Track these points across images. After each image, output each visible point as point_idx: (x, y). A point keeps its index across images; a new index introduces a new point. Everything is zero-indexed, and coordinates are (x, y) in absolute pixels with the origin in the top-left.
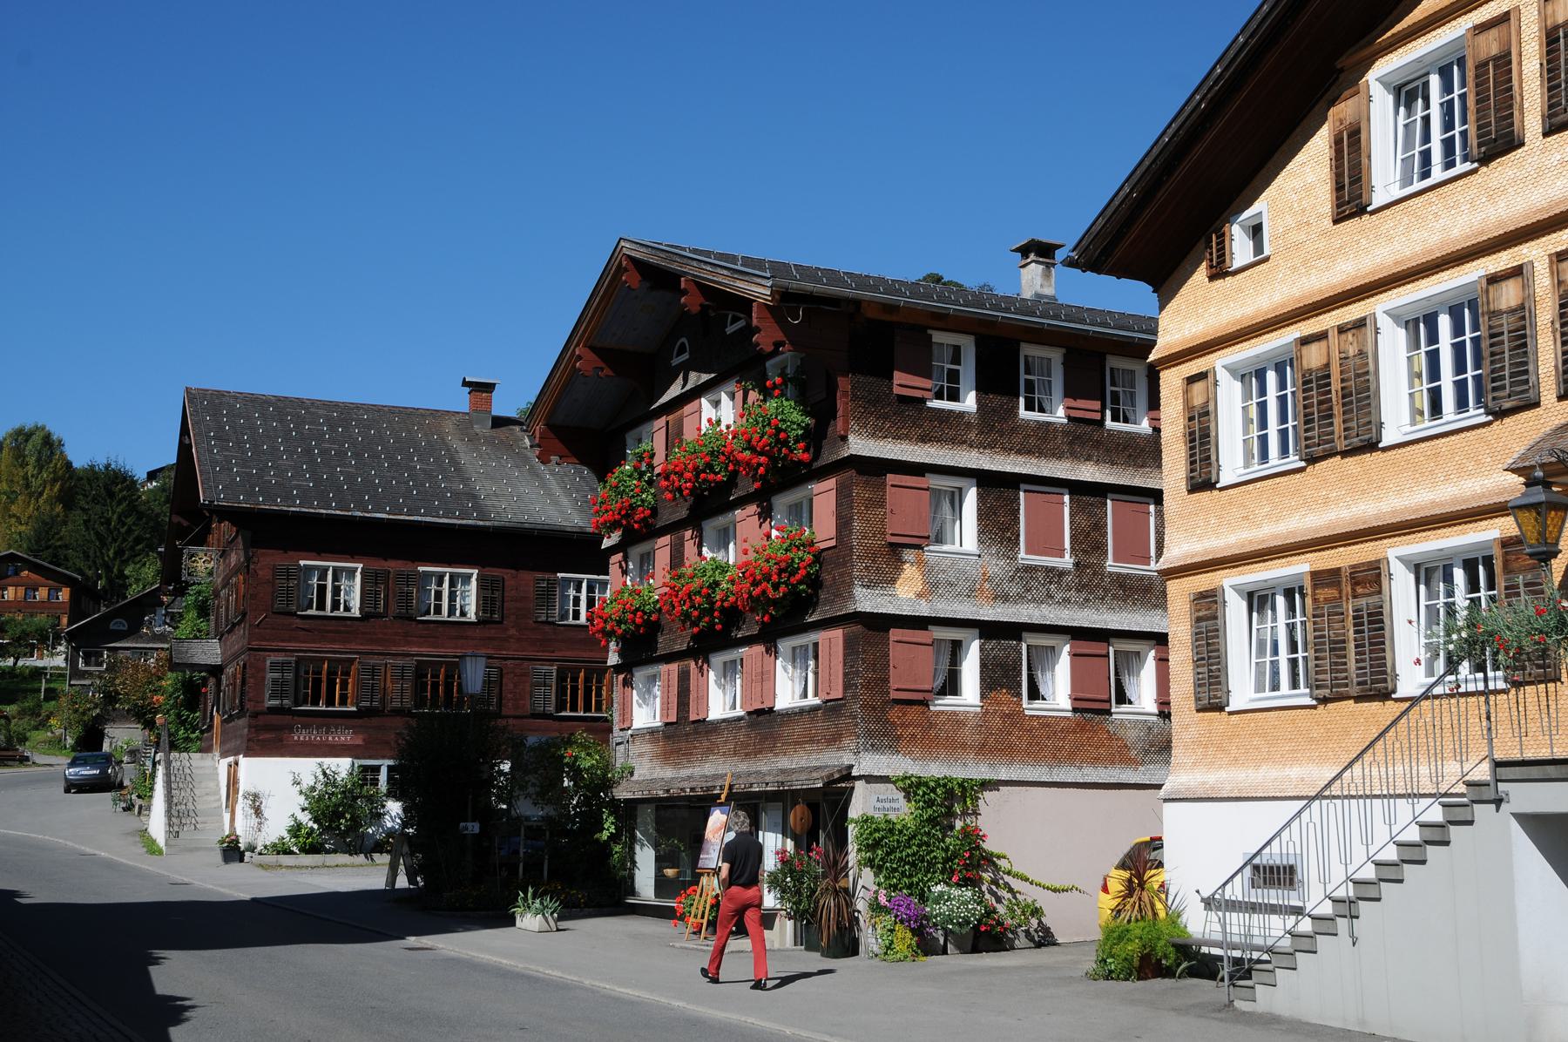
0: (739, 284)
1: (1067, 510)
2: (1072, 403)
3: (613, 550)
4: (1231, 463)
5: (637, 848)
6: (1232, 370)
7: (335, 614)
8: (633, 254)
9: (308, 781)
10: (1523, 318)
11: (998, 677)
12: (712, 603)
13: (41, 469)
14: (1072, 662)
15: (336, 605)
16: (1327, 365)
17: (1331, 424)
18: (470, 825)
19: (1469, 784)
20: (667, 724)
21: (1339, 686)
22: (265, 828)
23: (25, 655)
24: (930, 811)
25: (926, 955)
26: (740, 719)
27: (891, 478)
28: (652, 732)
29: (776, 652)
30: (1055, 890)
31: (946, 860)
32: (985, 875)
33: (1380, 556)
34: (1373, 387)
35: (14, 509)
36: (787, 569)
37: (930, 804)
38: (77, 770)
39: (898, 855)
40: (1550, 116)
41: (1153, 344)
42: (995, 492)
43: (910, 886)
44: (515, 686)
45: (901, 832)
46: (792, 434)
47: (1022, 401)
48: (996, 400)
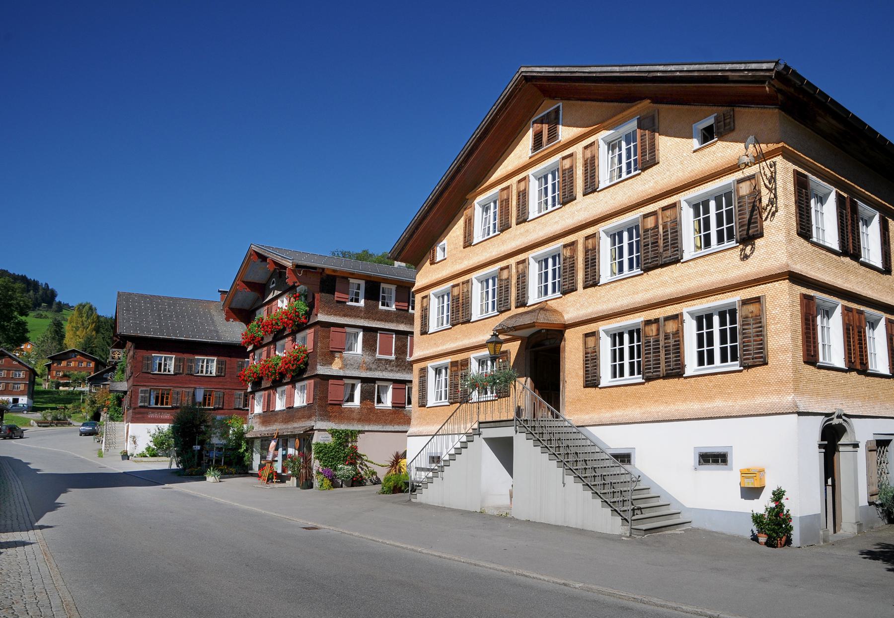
0: (283, 261)
1: (394, 340)
2: (398, 304)
3: (251, 352)
4: (433, 327)
5: (254, 454)
6: (435, 295)
7: (165, 373)
8: (255, 249)
9: (153, 432)
10: (508, 282)
11: (367, 396)
12: (276, 370)
13: (88, 318)
14: (393, 390)
15: (165, 370)
16: (459, 294)
17: (459, 314)
18: (196, 446)
19: (473, 429)
20: (264, 412)
21: (456, 399)
22: (137, 448)
23: (78, 386)
24: (339, 441)
25: (334, 488)
26: (284, 410)
27: (332, 329)
28: (260, 414)
29: (295, 387)
30: (382, 466)
31: (344, 457)
32: (358, 461)
33: (469, 357)
34: (470, 302)
35: (78, 333)
36: (296, 359)
37: (340, 438)
38: (84, 428)
39: (328, 455)
40: (518, 219)
41: (413, 284)
42: (369, 333)
43: (331, 466)
44: (229, 398)
45: (329, 447)
46: (301, 313)
47: (380, 303)
48: (371, 302)
